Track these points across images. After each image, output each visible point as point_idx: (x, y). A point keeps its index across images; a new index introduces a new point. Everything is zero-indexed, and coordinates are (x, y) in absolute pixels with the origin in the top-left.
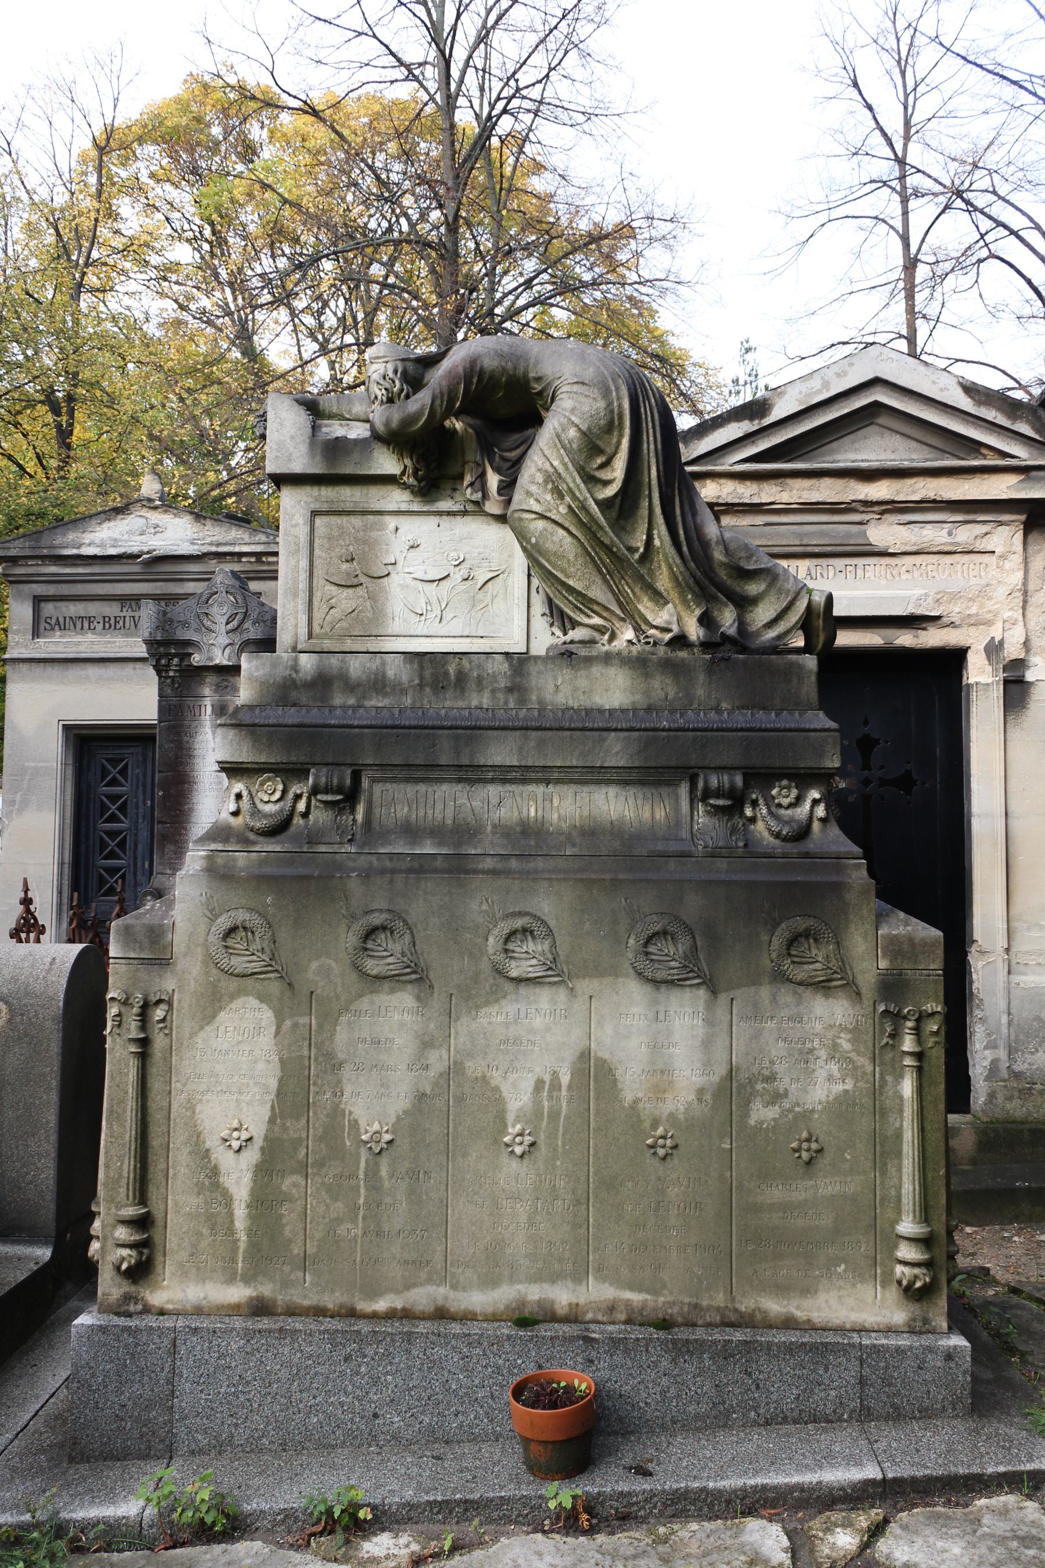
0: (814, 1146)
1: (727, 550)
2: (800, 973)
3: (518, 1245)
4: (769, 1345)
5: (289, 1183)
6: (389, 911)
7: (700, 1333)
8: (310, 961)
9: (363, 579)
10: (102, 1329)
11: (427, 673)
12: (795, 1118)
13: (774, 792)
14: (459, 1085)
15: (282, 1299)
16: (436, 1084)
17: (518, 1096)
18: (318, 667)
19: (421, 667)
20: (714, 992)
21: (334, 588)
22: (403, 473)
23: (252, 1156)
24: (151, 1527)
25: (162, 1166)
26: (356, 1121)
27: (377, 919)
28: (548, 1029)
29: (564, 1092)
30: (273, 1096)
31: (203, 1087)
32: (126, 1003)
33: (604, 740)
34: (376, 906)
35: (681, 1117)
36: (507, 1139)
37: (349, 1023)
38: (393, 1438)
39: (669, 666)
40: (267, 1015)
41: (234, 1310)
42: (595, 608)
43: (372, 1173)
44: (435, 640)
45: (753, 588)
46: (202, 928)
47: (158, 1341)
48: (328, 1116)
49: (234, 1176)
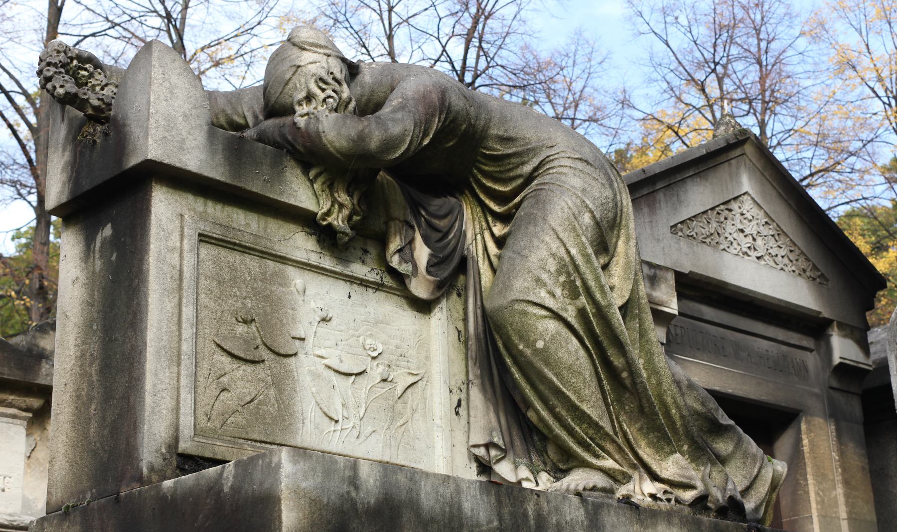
9: (265, 354)
21: (226, 359)
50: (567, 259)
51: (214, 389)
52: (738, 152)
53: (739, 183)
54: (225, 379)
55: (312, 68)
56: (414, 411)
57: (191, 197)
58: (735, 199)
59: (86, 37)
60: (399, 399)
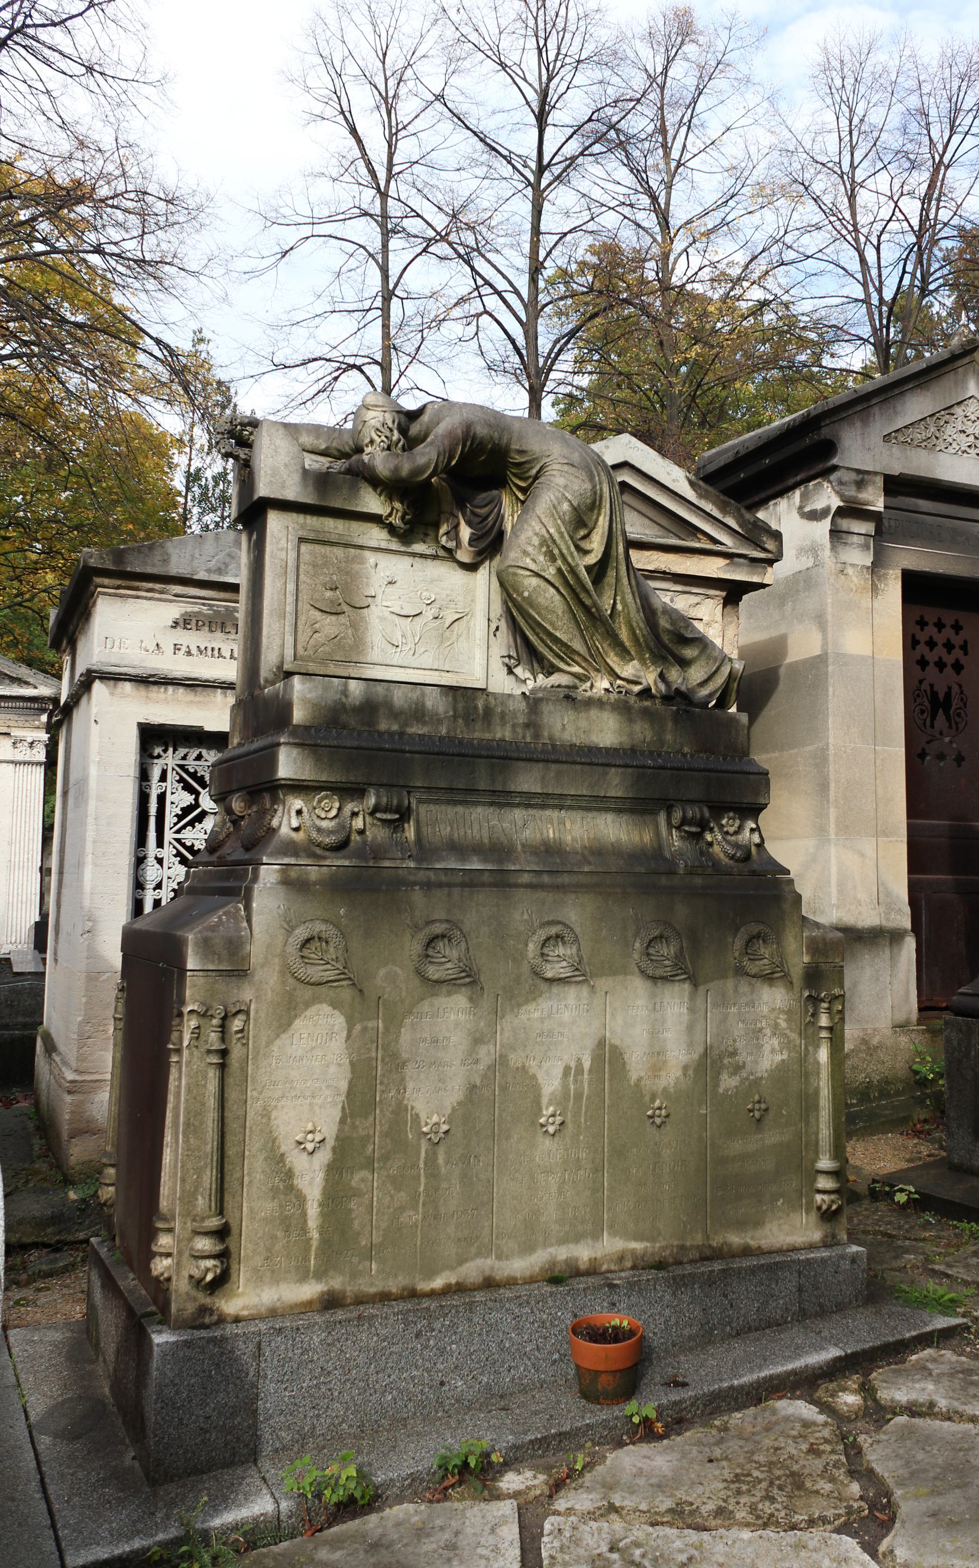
0: (763, 1106)
1: (673, 623)
2: (753, 968)
3: (550, 1213)
4: (740, 1269)
5: (357, 1179)
6: (447, 921)
7: (689, 1269)
8: (378, 968)
9: (345, 608)
10: (187, 1344)
11: (460, 706)
12: (750, 1085)
13: (724, 822)
14: (503, 1076)
15: (350, 1290)
16: (484, 1076)
17: (550, 1083)
18: (366, 693)
19: (455, 700)
20: (695, 985)
21: (318, 614)
22: (390, 515)
23: (324, 1156)
24: (290, 1517)
25: (237, 1175)
26: (417, 1115)
27: (438, 929)
28: (574, 1022)
29: (586, 1076)
30: (343, 1098)
31: (278, 1094)
32: (205, 1015)
33: (607, 774)
34: (436, 917)
35: (672, 1090)
36: (542, 1120)
37: (412, 1025)
38: (457, 1401)
39: (647, 714)
40: (339, 1021)
41: (306, 1307)
42: (576, 658)
43: (431, 1160)
44: (408, 671)
45: (689, 653)
46: (280, 939)
47: (243, 1347)
48: (393, 1112)
49: (307, 1178)
50: (547, 536)
51: (309, 632)
52: (967, 360)
53: (965, 388)
54: (317, 626)
55: (373, 422)
56: (459, 636)
57: (295, 515)
58: (959, 403)
59: (565, 234)
60: (449, 627)
